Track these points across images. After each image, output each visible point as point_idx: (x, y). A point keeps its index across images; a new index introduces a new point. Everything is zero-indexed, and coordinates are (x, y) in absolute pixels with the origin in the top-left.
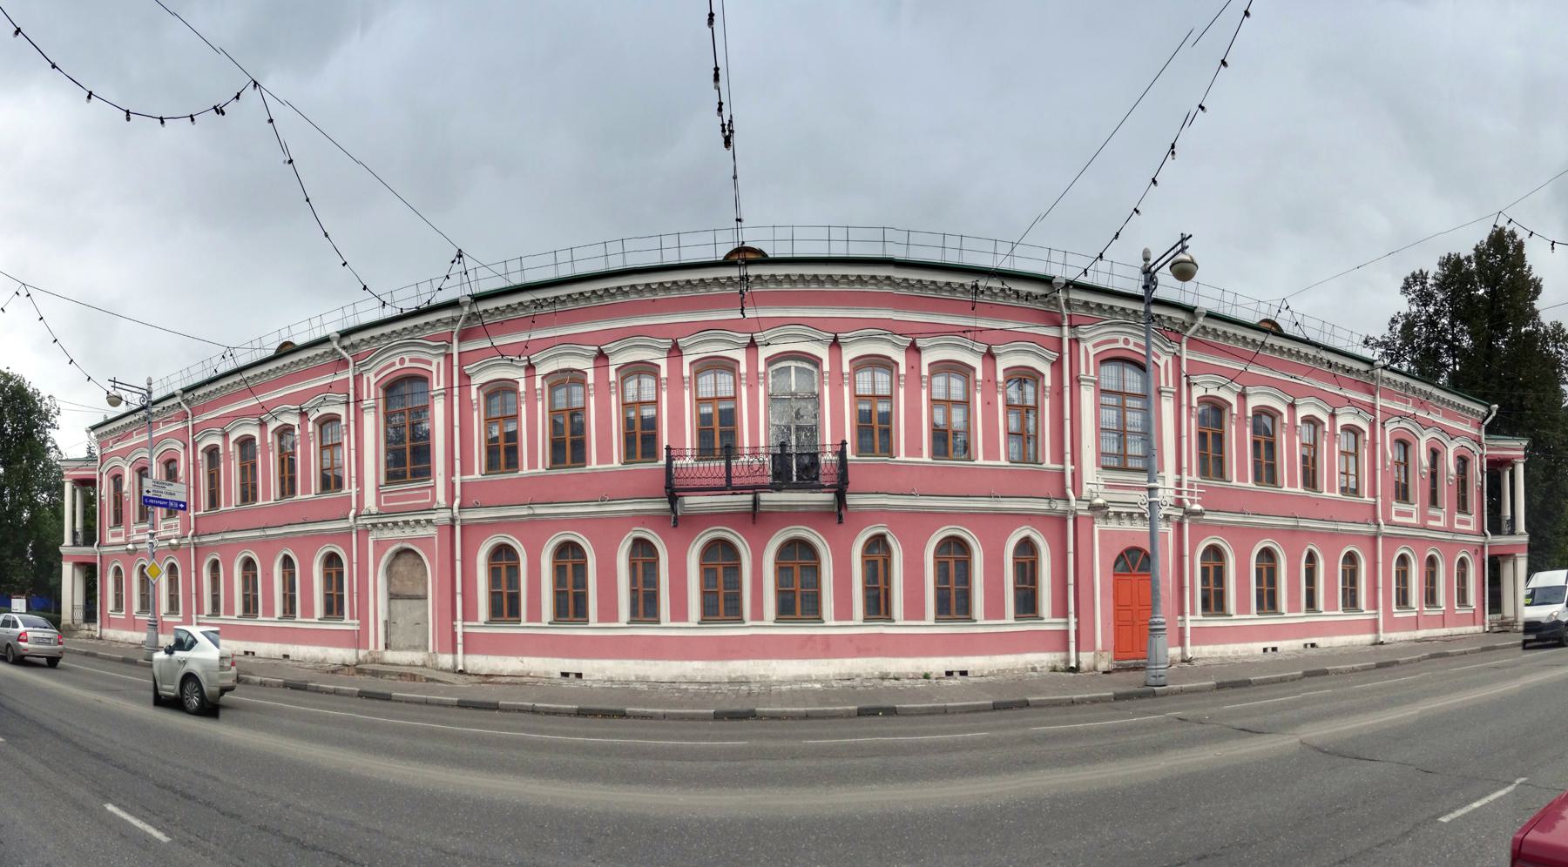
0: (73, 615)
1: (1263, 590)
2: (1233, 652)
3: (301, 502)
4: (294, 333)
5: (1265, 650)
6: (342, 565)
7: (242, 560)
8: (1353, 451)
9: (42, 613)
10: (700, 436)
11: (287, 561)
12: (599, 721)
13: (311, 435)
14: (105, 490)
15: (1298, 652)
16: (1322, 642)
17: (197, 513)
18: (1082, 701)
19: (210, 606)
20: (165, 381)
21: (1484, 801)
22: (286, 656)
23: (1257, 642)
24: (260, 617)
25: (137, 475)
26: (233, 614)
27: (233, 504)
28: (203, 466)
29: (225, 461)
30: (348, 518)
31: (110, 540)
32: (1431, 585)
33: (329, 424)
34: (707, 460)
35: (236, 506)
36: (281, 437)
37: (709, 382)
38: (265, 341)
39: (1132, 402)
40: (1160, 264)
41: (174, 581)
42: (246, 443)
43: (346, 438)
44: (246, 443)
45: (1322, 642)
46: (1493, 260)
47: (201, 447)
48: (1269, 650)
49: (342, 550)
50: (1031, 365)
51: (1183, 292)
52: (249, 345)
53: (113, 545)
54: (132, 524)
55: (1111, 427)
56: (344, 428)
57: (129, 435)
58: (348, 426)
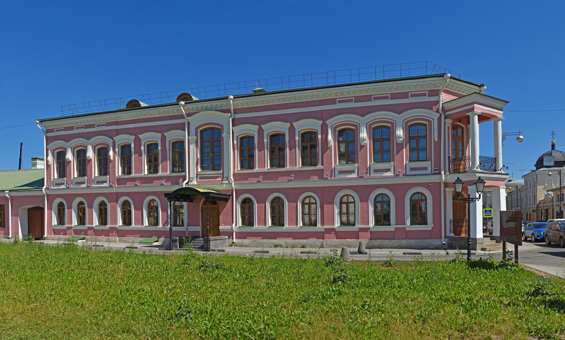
0: (560, 177)
1: (126, 217)
6: (64, 206)
8: (461, 150)
9: (465, 150)
10: (284, 157)
12: (414, 176)
14: (550, 210)
21: (10, 229)
22: (485, 254)
23: (471, 108)
32: (83, 215)
34: (377, 139)
37: (379, 132)
39: (520, 182)
40: (514, 134)
46: (436, 310)
49: (250, 195)
50: (374, 197)
51: (90, 108)
52: (434, 69)
55: (415, 135)
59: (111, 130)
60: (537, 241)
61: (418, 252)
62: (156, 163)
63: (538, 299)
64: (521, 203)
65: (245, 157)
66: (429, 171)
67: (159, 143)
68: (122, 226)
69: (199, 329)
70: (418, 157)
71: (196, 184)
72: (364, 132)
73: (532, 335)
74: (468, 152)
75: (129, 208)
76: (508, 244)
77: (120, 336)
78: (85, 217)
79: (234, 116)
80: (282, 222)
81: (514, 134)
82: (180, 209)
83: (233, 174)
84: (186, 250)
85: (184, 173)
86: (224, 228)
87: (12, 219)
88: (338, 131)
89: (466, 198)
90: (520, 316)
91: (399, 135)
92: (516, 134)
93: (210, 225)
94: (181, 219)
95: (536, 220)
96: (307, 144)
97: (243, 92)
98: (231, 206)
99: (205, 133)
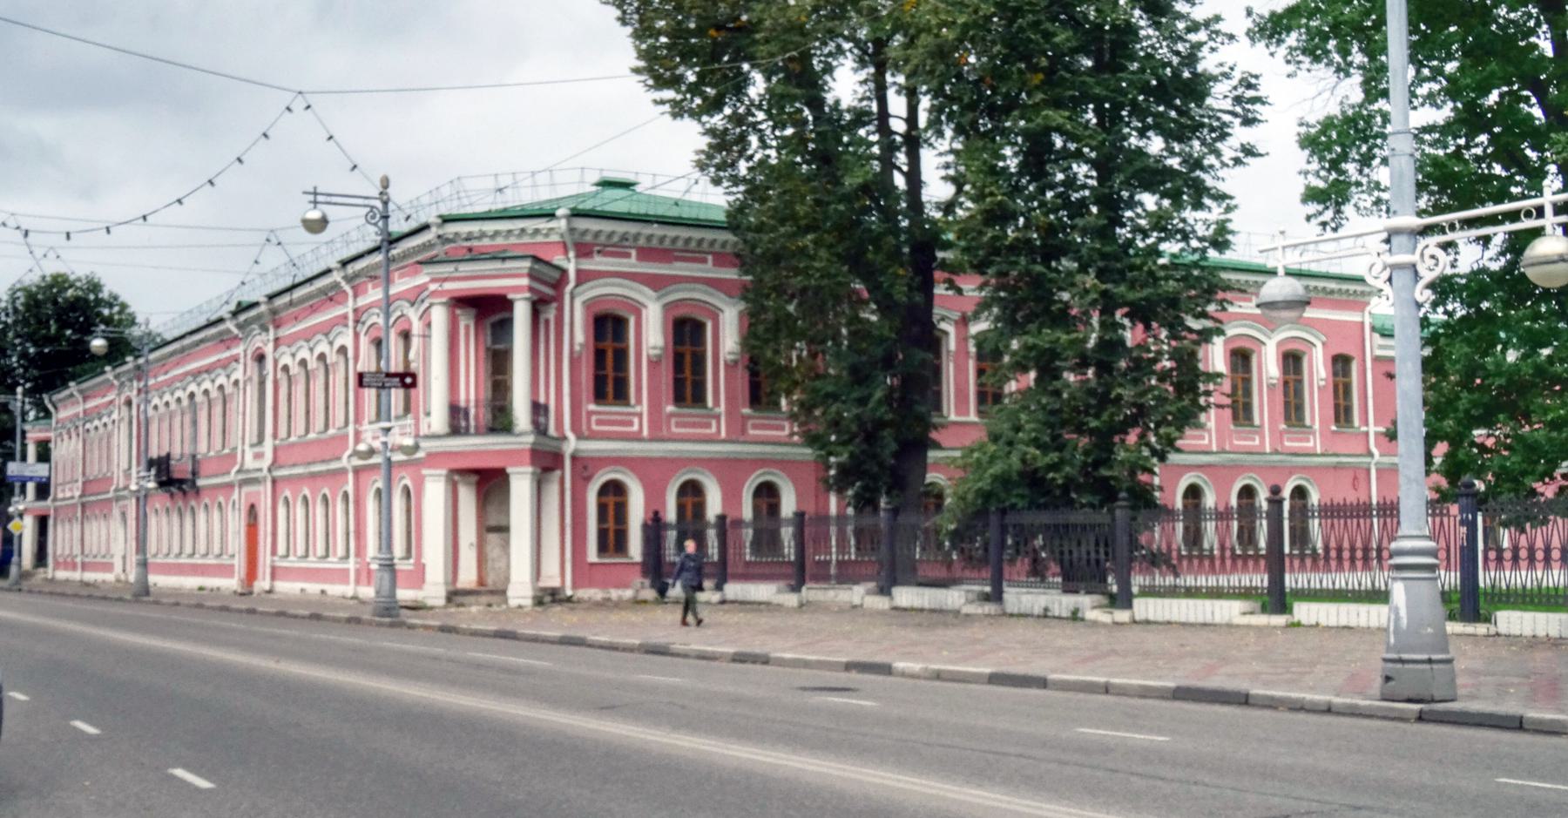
40: (334, 199)
60: (432, 608)
63: (1161, 47)
65: (662, 102)
66: (673, 421)
69: (1061, 545)
70: (551, 176)
73: (443, 244)
74: (189, 594)
76: (1494, 165)
77: (992, 380)
78: (1300, 381)
80: (1340, 366)
81: (334, 199)
82: (562, 596)
83: (645, 527)
84: (1331, 803)
85: (1107, 337)
86: (656, 264)
90: (1172, 384)
92: (329, 199)
93: (1174, 121)
98: (823, 685)
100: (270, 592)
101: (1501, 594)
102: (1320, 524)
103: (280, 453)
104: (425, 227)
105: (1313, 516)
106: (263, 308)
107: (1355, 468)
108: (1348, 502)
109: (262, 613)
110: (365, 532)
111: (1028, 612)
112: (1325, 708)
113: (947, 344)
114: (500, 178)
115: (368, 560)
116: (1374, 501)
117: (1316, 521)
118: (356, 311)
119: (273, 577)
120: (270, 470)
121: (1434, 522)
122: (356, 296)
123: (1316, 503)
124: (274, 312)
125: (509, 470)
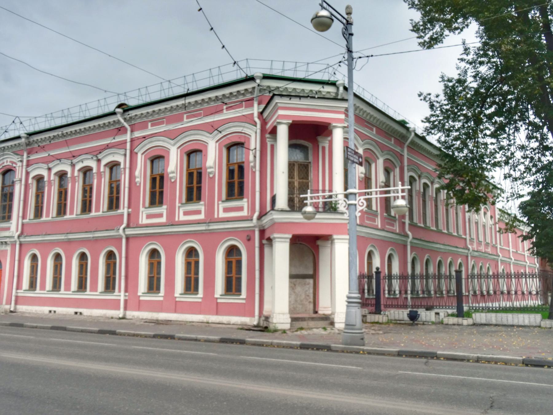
2: (35, 311)
3: (45, 223)
4: (108, 103)
5: (50, 311)
7: (149, 251)
11: (83, 256)
13: (122, 170)
15: (70, 315)
16: (86, 312)
17: (24, 221)
18: (141, 336)
19: (77, 285)
20: (83, 107)
24: (88, 292)
25: (185, 158)
26: (96, 291)
27: (28, 218)
28: (32, 188)
29: (48, 186)
30: (252, 220)
31: (143, 220)
33: (235, 147)
35: (29, 220)
36: (111, 169)
38: (252, 64)
41: (84, 266)
42: (62, 175)
43: (123, 176)
44: (62, 175)
45: (86, 312)
47: (32, 175)
48: (52, 312)
53: (228, 220)
54: (177, 204)
56: (122, 170)
57: (179, 119)
58: (125, 169)
59: (333, 118)
61: (144, 148)
62: (114, 276)
64: (424, 155)
67: (407, 214)
68: (318, 13)
71: (398, 231)
72: (120, 291)
75: (481, 20)
79: (17, 293)
87: (46, 234)
88: (272, 219)
89: (539, 146)
91: (395, 274)
94: (120, 281)
95: (412, 241)
96: (295, 178)
97: (417, 237)
99: (523, 256)
100: (124, 318)
101: (522, 308)
102: (420, 281)
103: (25, 228)
104: (251, 79)
105: (417, 278)
106: (23, 140)
107: (494, 259)
108: (520, 272)
109: (180, 339)
110: (22, 280)
111: (402, 319)
112: (270, 344)
113: (429, 192)
114: (71, 110)
115: (139, 294)
116: (513, 272)
117: (419, 280)
118: (132, 140)
119: (16, 303)
120: (19, 237)
121: (400, 282)
122: (132, 131)
123: (419, 273)
124: (28, 144)
125: (335, 237)
